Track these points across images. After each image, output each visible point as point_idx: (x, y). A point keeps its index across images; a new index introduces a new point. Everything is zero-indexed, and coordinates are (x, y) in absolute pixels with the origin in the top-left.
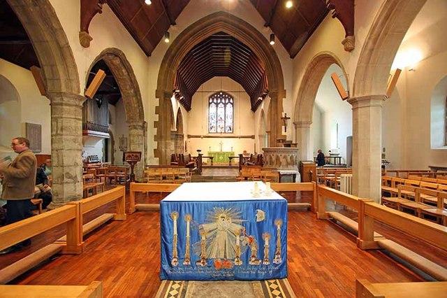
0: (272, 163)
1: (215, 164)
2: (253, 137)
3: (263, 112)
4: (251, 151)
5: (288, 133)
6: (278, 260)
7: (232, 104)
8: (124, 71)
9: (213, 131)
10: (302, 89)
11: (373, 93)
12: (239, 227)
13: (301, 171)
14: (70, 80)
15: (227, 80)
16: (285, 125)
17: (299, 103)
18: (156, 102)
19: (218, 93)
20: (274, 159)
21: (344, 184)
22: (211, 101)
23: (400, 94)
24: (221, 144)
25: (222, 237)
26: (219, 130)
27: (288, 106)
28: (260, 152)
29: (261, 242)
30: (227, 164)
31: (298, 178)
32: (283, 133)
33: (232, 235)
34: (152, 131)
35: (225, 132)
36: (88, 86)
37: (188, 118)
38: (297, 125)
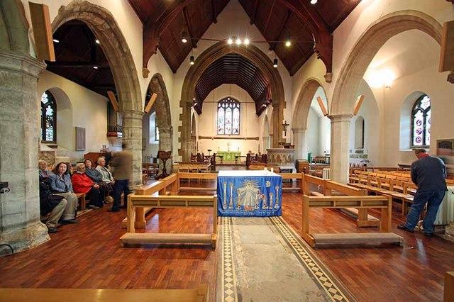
0: (274, 161)
1: (224, 163)
2: (257, 139)
3: (266, 117)
4: (255, 152)
5: (288, 137)
6: (277, 207)
7: (239, 109)
8: (160, 88)
9: (221, 132)
10: (299, 103)
11: (343, 113)
12: (258, 190)
13: (297, 167)
14: (137, 102)
15: (234, 86)
16: (285, 130)
17: (296, 113)
18: (180, 110)
19: (226, 99)
20: (275, 157)
21: (325, 175)
22: (220, 106)
23: (379, 108)
24: (228, 145)
25: (248, 195)
26: (226, 133)
27: (287, 115)
28: (263, 152)
29: (269, 198)
30: (234, 163)
31: (294, 172)
32: (284, 137)
33: (253, 194)
34: (177, 134)
35: (224, 134)
36: (146, 105)
37: (199, 120)
38: (294, 131)
